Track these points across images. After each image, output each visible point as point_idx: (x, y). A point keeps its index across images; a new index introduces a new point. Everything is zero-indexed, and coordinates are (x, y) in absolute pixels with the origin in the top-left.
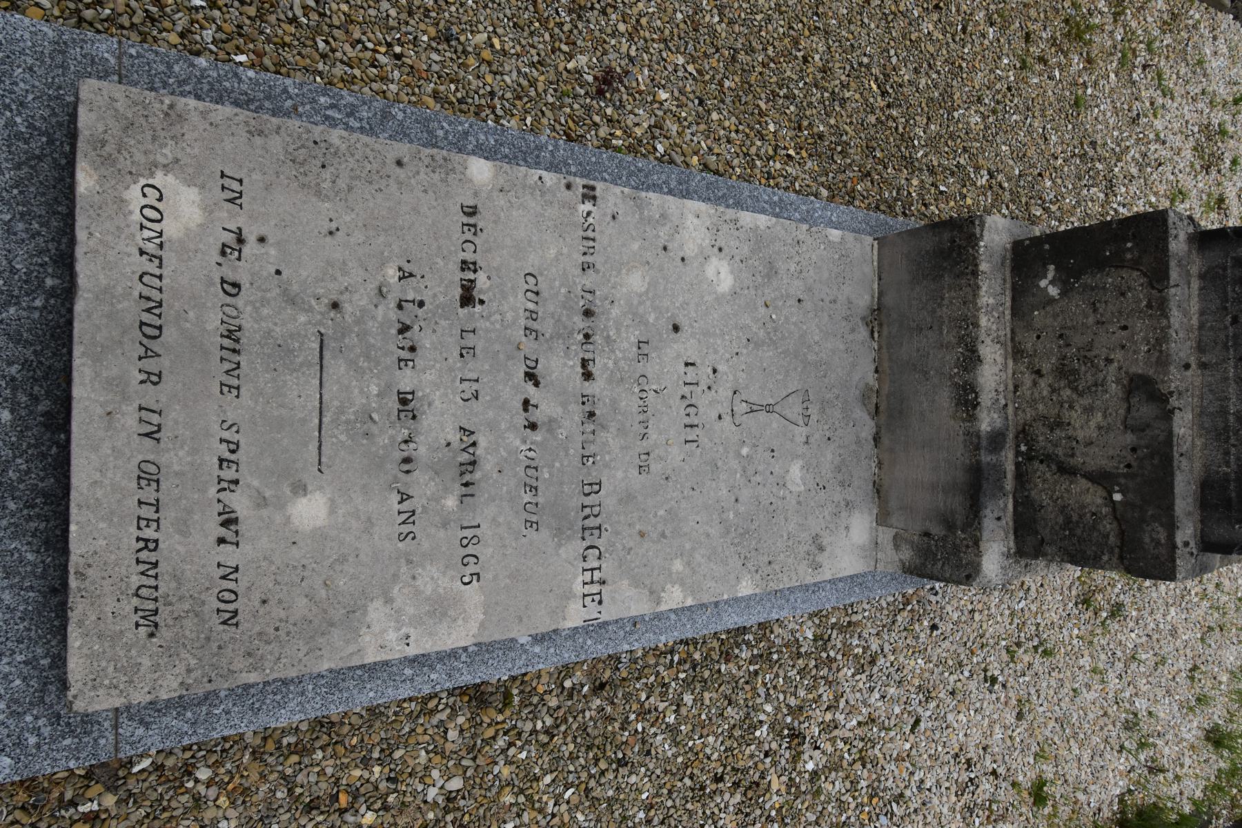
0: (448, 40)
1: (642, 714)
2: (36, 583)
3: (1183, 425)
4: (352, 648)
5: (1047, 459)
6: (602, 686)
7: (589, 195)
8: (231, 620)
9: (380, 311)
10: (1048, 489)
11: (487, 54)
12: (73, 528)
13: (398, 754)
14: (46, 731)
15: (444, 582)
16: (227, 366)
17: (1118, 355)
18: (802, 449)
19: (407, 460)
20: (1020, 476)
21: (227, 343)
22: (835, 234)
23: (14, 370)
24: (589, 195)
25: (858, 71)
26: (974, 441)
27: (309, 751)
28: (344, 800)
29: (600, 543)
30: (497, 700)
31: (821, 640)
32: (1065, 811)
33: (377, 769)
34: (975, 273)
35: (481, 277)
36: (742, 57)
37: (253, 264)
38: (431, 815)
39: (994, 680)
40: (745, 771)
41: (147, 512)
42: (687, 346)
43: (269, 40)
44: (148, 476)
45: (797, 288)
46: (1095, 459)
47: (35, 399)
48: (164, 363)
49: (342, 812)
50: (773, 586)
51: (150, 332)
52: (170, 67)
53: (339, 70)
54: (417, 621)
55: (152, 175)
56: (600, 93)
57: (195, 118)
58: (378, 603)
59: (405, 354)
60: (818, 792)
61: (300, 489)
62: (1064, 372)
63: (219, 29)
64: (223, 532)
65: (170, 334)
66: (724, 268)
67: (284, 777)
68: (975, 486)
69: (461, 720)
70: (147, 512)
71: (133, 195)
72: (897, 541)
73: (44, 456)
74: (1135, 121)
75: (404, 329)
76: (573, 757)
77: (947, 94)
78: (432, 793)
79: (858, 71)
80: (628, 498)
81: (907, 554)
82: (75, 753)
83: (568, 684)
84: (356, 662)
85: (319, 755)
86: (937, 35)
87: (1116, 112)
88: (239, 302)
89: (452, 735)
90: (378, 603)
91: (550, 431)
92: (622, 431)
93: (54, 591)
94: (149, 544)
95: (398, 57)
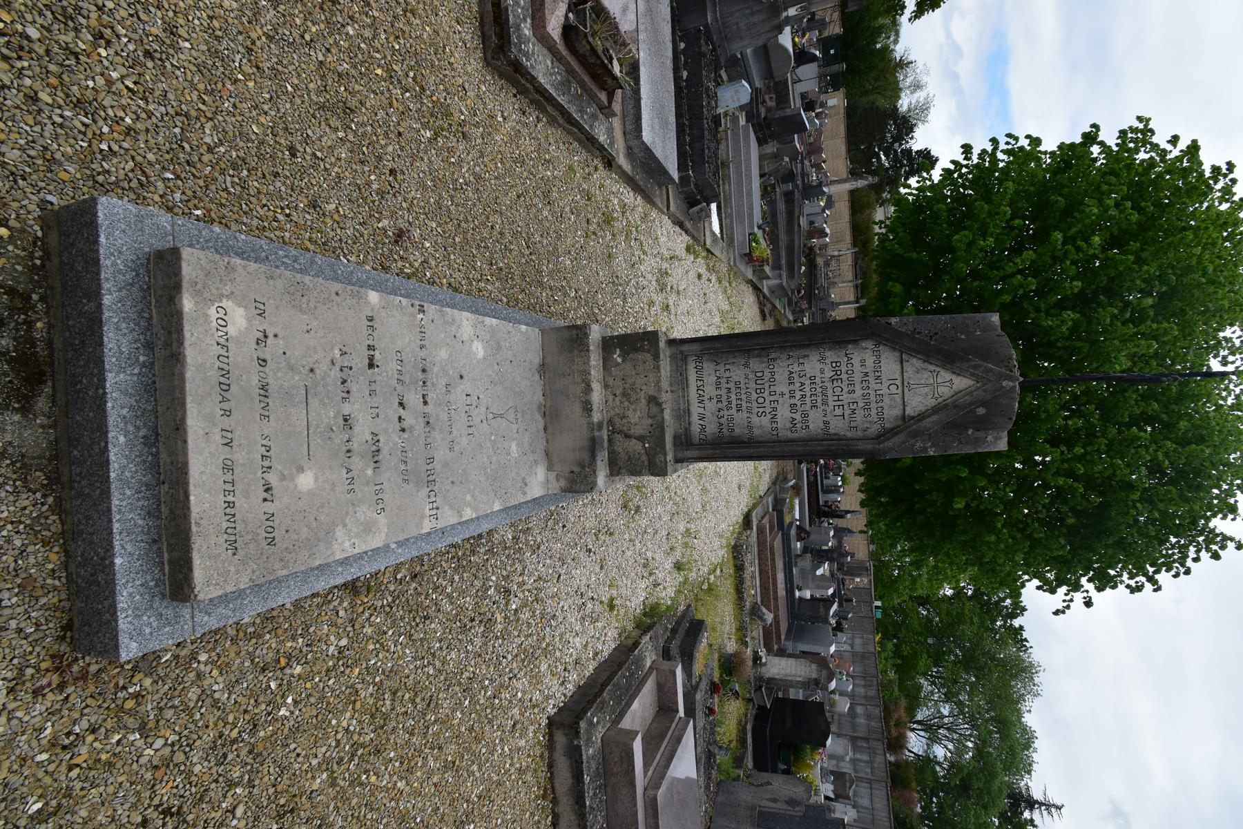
0: (314, 207)
1: (436, 588)
2: (144, 537)
3: (667, 415)
4: (329, 553)
5: (620, 432)
6: (416, 576)
7: (422, 310)
8: (272, 542)
9: (333, 373)
10: (621, 445)
11: (336, 217)
12: (192, 498)
13: (311, 630)
14: (155, 624)
15: (369, 514)
16: (263, 405)
17: (644, 387)
18: (515, 436)
19: (349, 451)
20: (609, 441)
21: (262, 392)
22: (523, 327)
23: (125, 411)
24: (422, 310)
25: (516, 234)
26: (591, 426)
27: (260, 636)
28: (283, 662)
29: (435, 488)
30: (364, 590)
31: (516, 539)
32: (622, 611)
33: (300, 640)
34: (588, 351)
35: (377, 353)
36: (463, 224)
37: (273, 349)
38: (331, 663)
39: (590, 550)
40: (485, 614)
41: (228, 487)
42: (465, 386)
43: (211, 201)
44: (228, 467)
45: (509, 355)
46: (638, 431)
47: (138, 428)
48: (232, 404)
49: (282, 669)
50: (508, 505)
51: (225, 388)
52: (200, 232)
53: (255, 222)
54: (358, 535)
55: (221, 301)
56: (396, 242)
57: (240, 269)
58: (340, 528)
59: (345, 395)
60: (518, 620)
61: (301, 469)
62: (625, 394)
63: (183, 193)
64: (265, 495)
65: (234, 388)
66: (480, 346)
67: (249, 653)
68: (593, 446)
69: (345, 604)
70: (228, 487)
71: (212, 312)
72: (558, 478)
73: (144, 461)
74: (633, 266)
75: (344, 382)
76: (402, 618)
77: (556, 249)
78: (332, 648)
79: (516, 234)
80: (446, 465)
81: (563, 483)
82: (172, 636)
83: (399, 577)
84: (331, 560)
85: (268, 636)
86: (550, 218)
87: (625, 261)
88: (267, 369)
89: (342, 613)
90: (340, 528)
91: (411, 432)
92: (441, 431)
93: (155, 541)
94: (230, 504)
95: (288, 216)
